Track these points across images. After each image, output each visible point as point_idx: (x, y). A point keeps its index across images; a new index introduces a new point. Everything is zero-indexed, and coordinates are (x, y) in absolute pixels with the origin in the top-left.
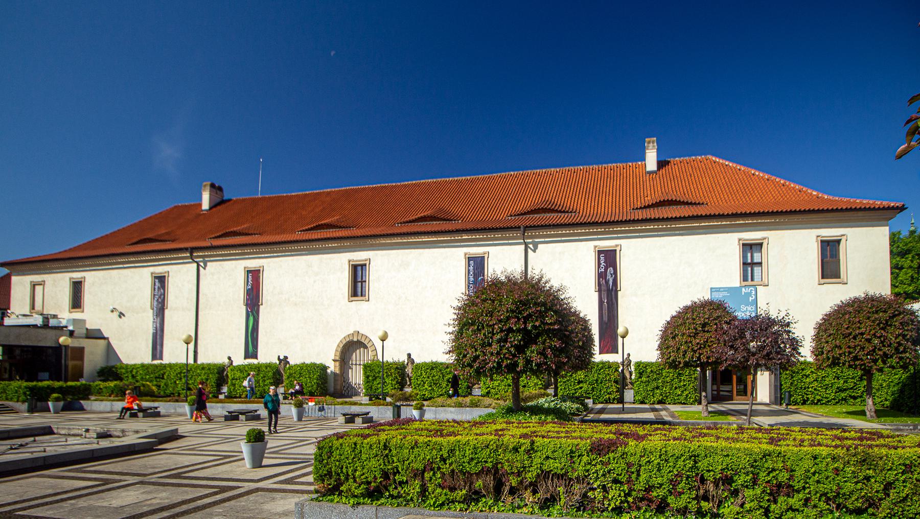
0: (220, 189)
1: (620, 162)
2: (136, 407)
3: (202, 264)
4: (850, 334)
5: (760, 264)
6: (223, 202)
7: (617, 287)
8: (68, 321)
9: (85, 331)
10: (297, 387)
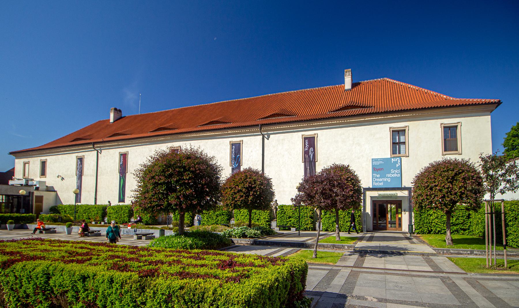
0: (120, 111)
1: (332, 85)
2: (42, 228)
3: (266, 136)
4: (428, 186)
5: (404, 143)
6: (121, 118)
7: (315, 160)
9: (45, 187)
10: (138, 218)
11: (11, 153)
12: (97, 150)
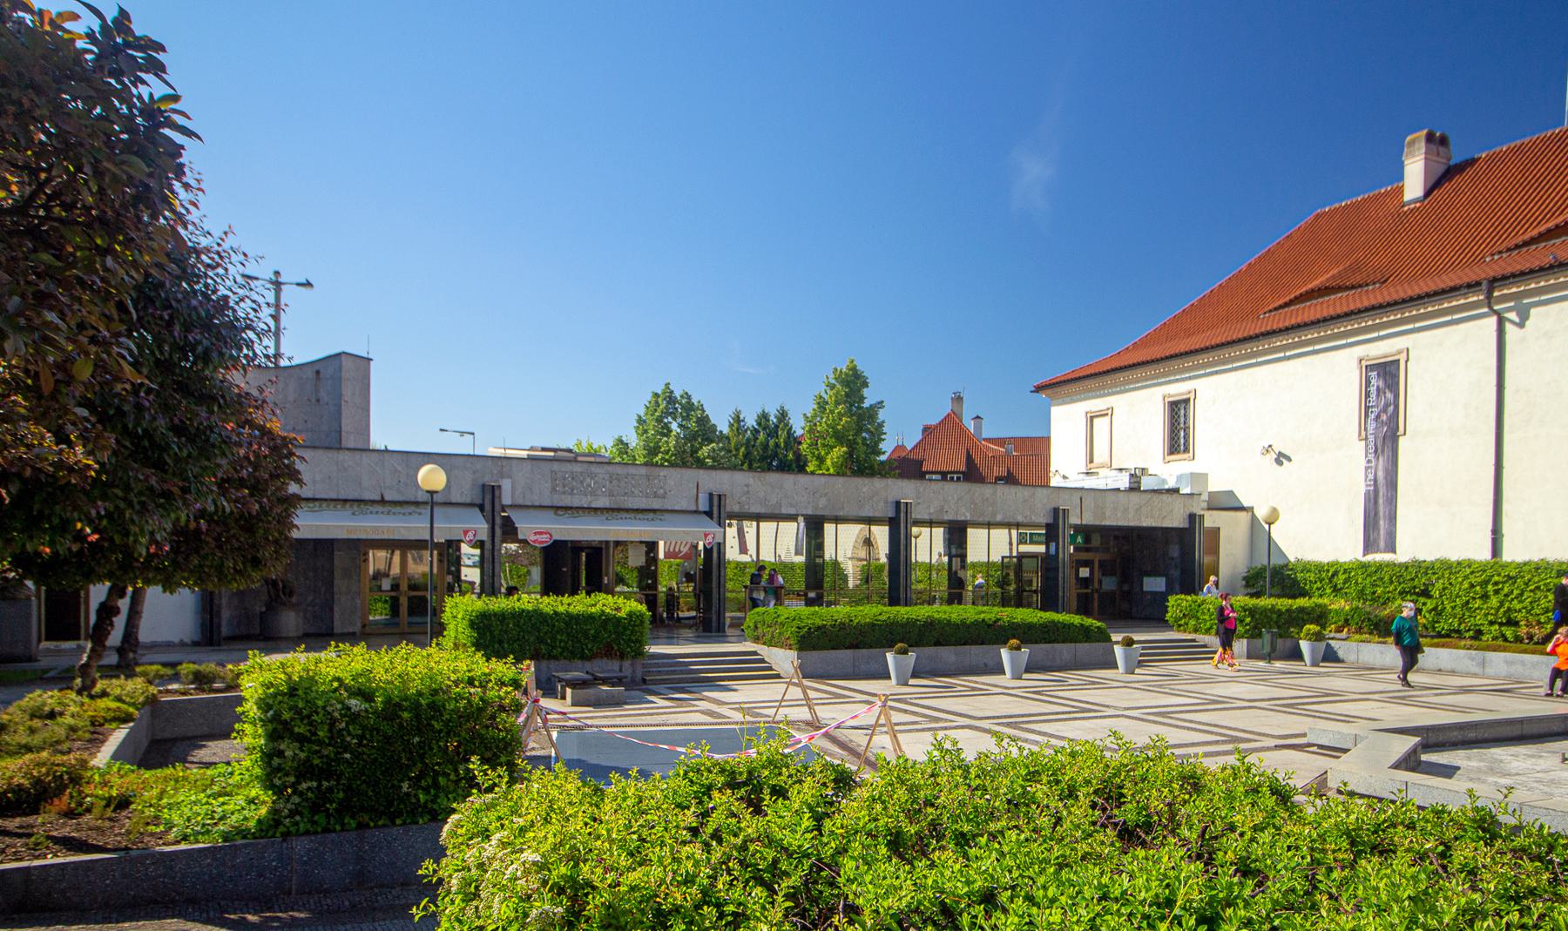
3: (1513, 316)
6: (1450, 173)
8: (1180, 478)
11: (1039, 389)
12: (1496, 312)
